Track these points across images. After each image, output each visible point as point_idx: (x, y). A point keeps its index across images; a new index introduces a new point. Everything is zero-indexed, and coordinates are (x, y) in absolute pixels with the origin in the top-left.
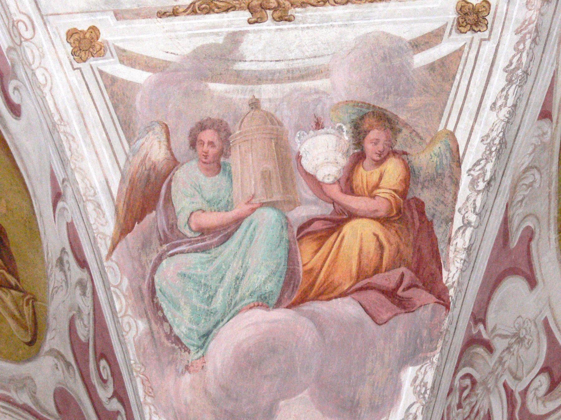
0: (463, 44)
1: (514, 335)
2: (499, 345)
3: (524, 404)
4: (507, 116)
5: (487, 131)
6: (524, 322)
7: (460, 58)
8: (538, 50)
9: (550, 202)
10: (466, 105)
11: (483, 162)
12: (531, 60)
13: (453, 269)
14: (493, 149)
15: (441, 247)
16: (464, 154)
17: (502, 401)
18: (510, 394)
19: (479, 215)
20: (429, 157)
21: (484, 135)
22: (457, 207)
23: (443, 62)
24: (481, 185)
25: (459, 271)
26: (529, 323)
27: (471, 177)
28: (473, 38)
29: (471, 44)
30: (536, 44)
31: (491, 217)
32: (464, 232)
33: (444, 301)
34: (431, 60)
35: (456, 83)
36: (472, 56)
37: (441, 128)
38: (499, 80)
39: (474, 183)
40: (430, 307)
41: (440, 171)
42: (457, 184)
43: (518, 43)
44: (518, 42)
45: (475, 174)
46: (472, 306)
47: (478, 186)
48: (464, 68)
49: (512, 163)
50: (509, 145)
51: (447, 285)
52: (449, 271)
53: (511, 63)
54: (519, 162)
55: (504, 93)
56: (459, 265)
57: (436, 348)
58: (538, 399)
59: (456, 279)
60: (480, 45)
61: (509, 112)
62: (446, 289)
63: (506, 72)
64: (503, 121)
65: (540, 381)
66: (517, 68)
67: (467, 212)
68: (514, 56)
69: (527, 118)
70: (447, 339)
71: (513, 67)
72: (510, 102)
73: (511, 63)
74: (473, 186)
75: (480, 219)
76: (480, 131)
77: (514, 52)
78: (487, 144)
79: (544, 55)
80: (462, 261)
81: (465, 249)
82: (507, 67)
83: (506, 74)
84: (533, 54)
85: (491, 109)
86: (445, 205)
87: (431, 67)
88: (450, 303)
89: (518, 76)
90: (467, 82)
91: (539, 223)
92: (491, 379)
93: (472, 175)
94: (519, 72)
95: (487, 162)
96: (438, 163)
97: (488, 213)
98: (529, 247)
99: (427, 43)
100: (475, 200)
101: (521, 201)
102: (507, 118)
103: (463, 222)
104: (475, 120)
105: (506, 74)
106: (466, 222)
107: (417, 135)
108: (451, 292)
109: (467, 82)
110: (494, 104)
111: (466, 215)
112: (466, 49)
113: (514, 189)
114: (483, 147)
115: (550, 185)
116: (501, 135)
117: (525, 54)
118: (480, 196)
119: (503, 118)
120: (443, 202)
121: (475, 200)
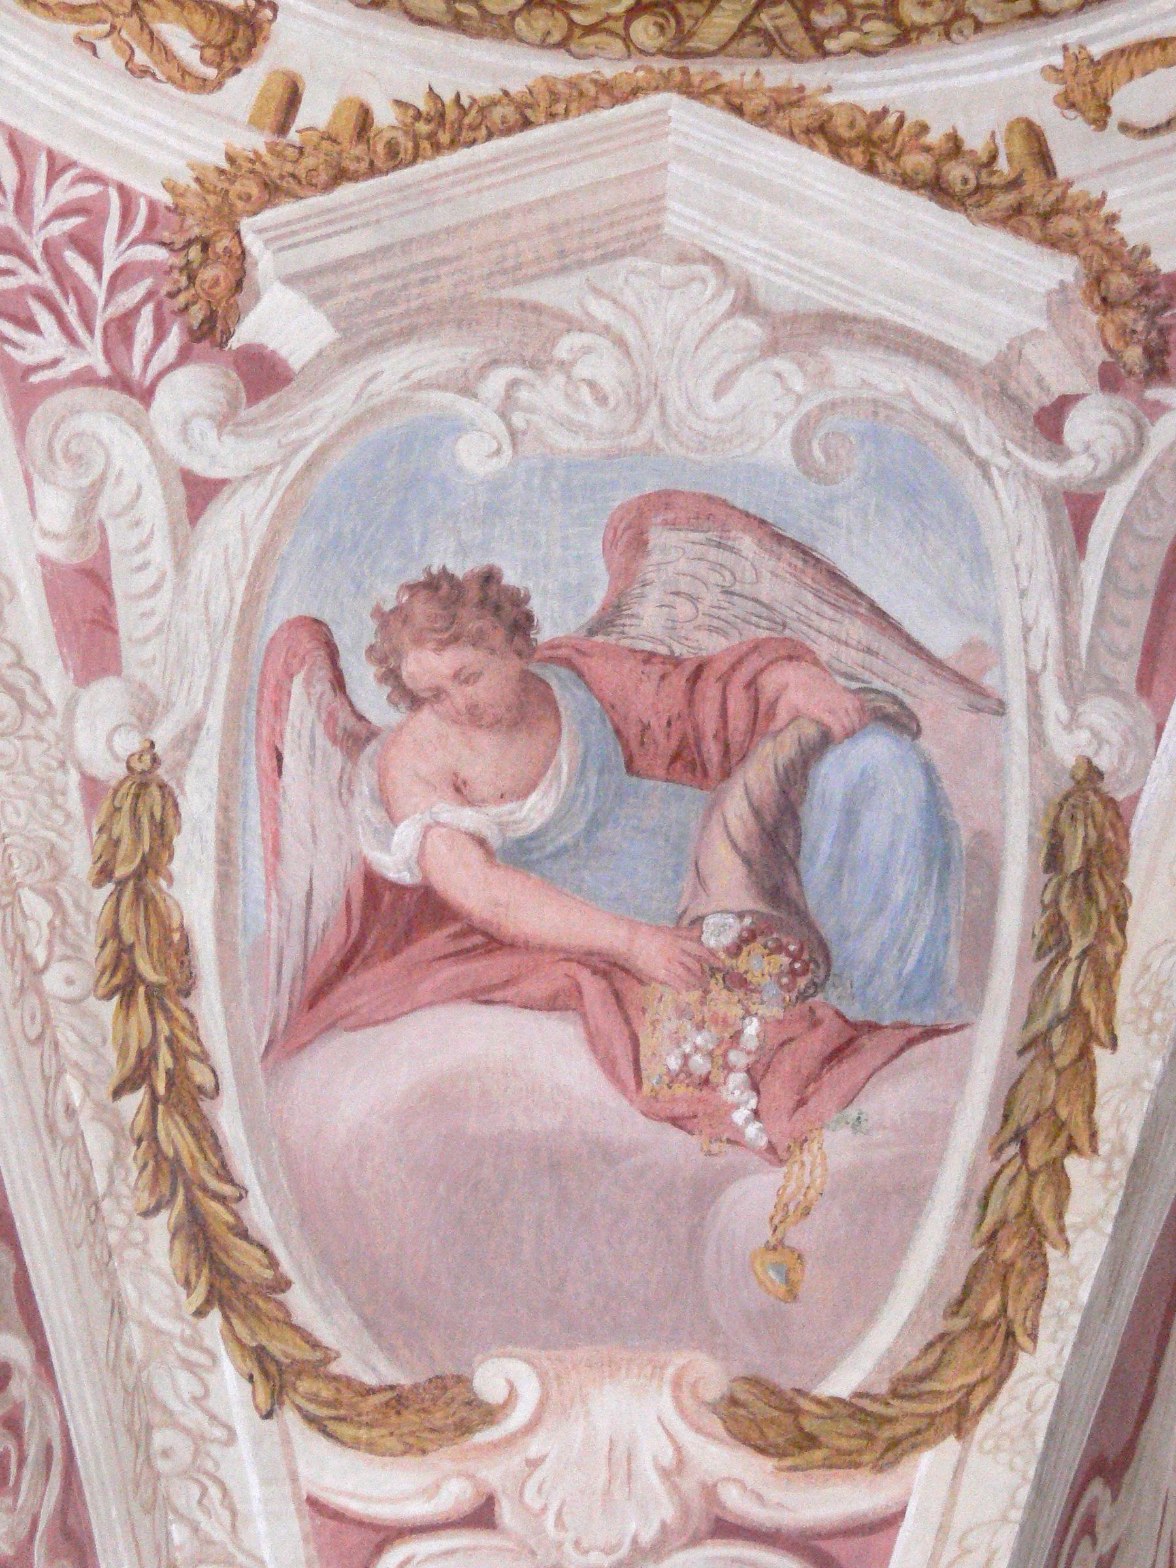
62: (1067, 503)
118: (753, 1009)
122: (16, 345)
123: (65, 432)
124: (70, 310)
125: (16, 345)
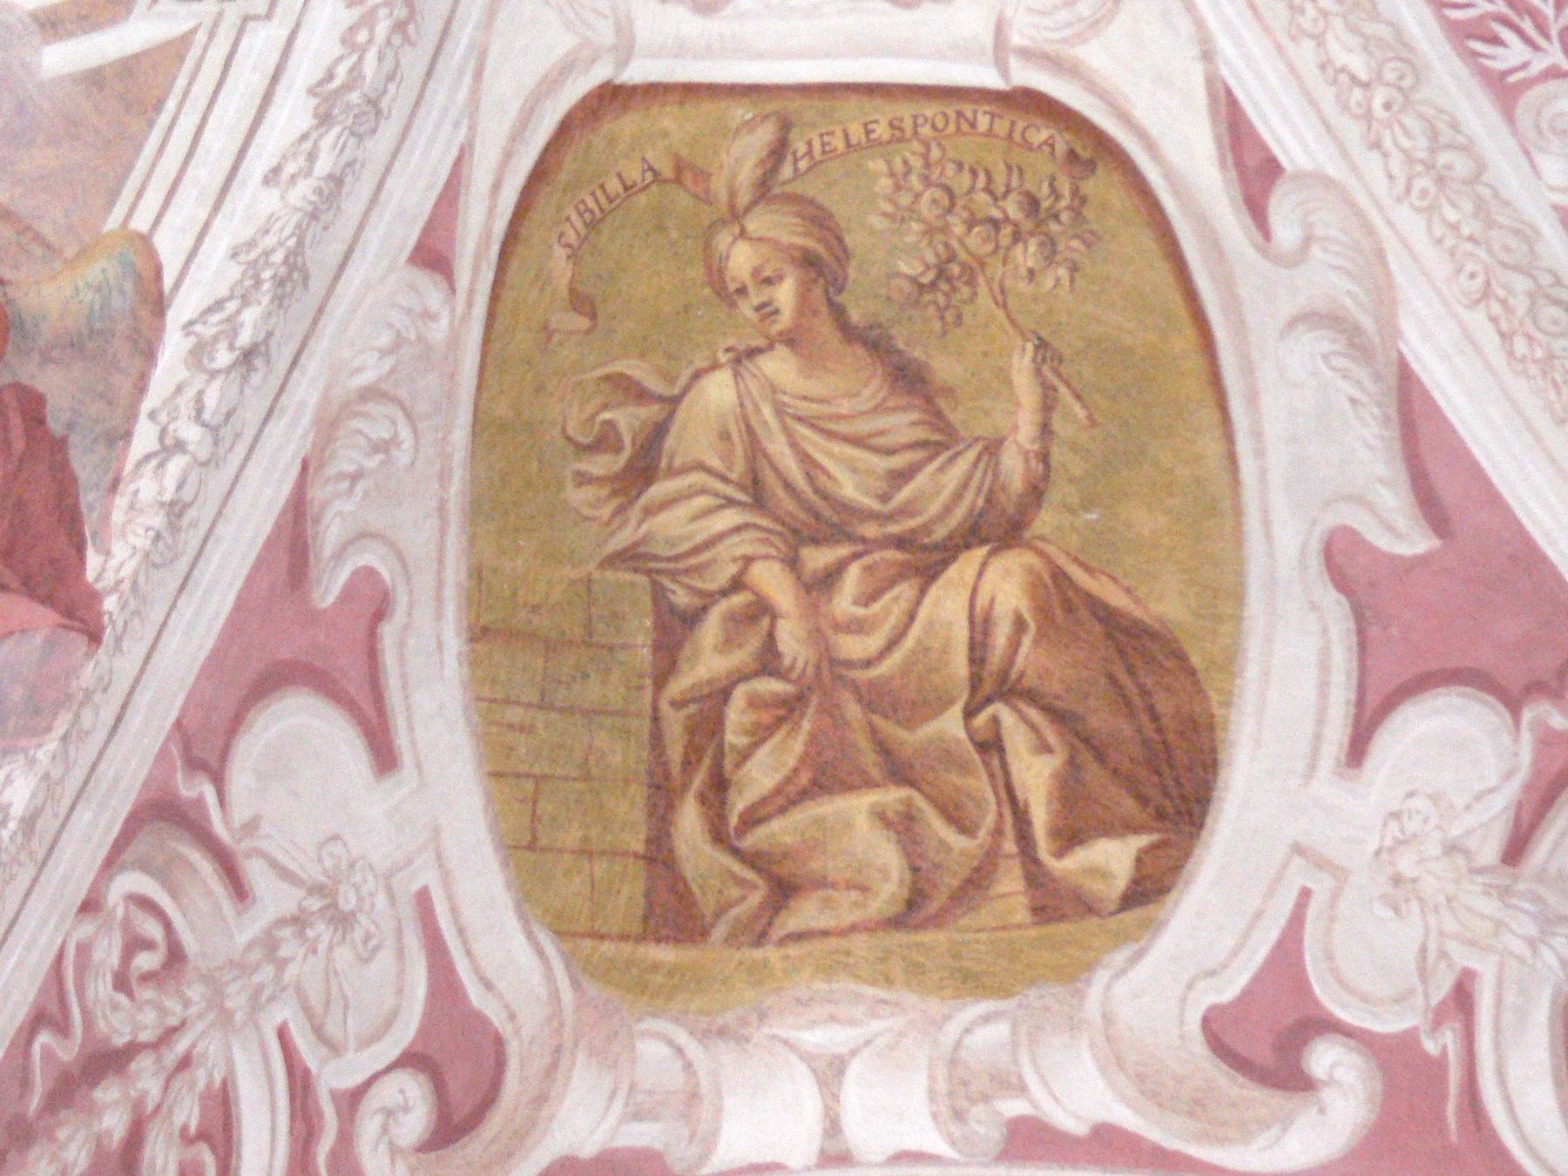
0: (192, 24)
1: (317, 889)
2: (274, 898)
3: (346, 1139)
4: (314, 198)
5: (248, 233)
6: (352, 865)
7: (182, 59)
8: (413, 62)
9: (443, 532)
10: (190, 172)
11: (232, 306)
12: (390, 78)
13: (120, 550)
14: (267, 274)
15: (88, 498)
16: (177, 285)
17: (272, 1093)
18: (300, 1083)
19: (214, 430)
20: (69, 292)
21: (241, 240)
22: (147, 405)
23: (128, 67)
24: (224, 357)
25: (138, 557)
26: (370, 878)
27: (192, 340)
28: (220, 15)
29: (216, 25)
30: (407, 39)
31: (251, 464)
32: (161, 465)
33: (82, 620)
34: (93, 61)
35: (164, 119)
36: (217, 54)
37: (112, 223)
38: (292, 114)
39: (199, 353)
40: (38, 639)
41: (98, 325)
42: (150, 356)
43: (353, 29)
44: (351, 28)
45: (207, 331)
46: (179, 702)
47: (212, 359)
48: (190, 84)
49: (320, 347)
50: (318, 284)
51: (99, 586)
52: (108, 553)
53: (330, 76)
54: (346, 354)
55: (307, 145)
56: (141, 541)
57: (48, 729)
58: (394, 1151)
59: (126, 572)
60: (241, 32)
61: (319, 191)
62: (95, 597)
63: (316, 95)
64: (297, 209)
65: (402, 1091)
66: (347, 87)
67: (175, 419)
68: (340, 59)
69: (374, 238)
70: (86, 722)
71: (337, 83)
72: (324, 165)
73: (330, 76)
74: (200, 360)
75: (216, 444)
76: (227, 232)
77: (338, 50)
78: (249, 263)
79: (431, 84)
80: (151, 534)
81: (162, 505)
82: (320, 83)
83: (316, 101)
84: (398, 64)
85: (267, 181)
86: (110, 403)
87: (94, 79)
88: (103, 628)
89: (348, 107)
90: (196, 120)
91: (409, 579)
92: (239, 983)
93: (197, 335)
94: (354, 97)
95: (245, 301)
96: (97, 307)
97: (241, 450)
98: (372, 636)
99: (85, 17)
100: (200, 393)
101: (355, 478)
102: (311, 203)
103: (161, 439)
104: (217, 207)
105: (316, 101)
106: (169, 441)
107: (38, 238)
108: (110, 604)
109: (196, 119)
110: (276, 170)
111: (171, 428)
112: (201, 37)
113: (328, 426)
114: (235, 271)
115: (444, 476)
116: (292, 242)
117: (371, 56)
118: (216, 384)
119: (299, 204)
120: (102, 395)
121: (200, 393)
122: (1488, 57)
123: (1548, 113)
124: (1527, 26)
125: (1488, 57)
